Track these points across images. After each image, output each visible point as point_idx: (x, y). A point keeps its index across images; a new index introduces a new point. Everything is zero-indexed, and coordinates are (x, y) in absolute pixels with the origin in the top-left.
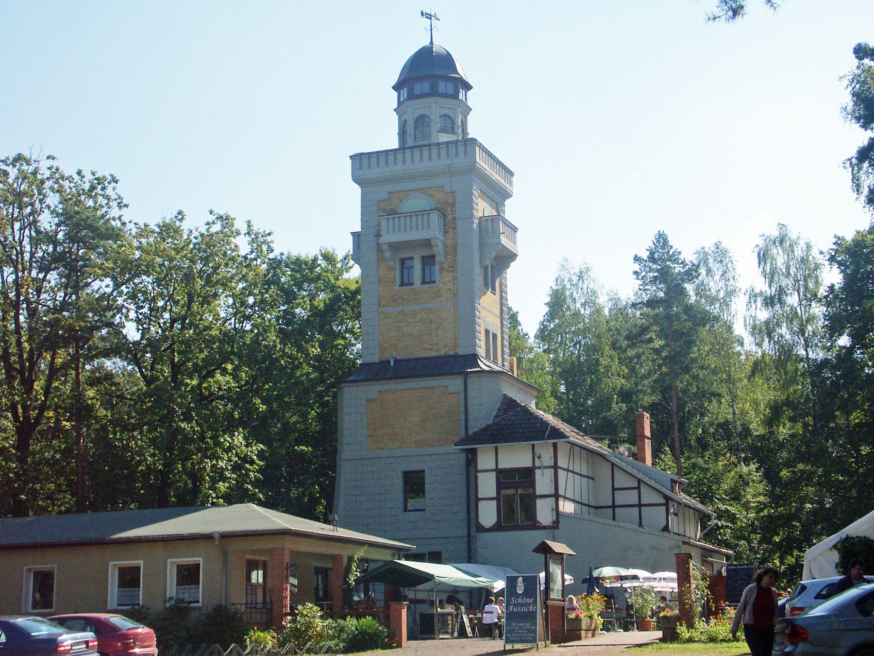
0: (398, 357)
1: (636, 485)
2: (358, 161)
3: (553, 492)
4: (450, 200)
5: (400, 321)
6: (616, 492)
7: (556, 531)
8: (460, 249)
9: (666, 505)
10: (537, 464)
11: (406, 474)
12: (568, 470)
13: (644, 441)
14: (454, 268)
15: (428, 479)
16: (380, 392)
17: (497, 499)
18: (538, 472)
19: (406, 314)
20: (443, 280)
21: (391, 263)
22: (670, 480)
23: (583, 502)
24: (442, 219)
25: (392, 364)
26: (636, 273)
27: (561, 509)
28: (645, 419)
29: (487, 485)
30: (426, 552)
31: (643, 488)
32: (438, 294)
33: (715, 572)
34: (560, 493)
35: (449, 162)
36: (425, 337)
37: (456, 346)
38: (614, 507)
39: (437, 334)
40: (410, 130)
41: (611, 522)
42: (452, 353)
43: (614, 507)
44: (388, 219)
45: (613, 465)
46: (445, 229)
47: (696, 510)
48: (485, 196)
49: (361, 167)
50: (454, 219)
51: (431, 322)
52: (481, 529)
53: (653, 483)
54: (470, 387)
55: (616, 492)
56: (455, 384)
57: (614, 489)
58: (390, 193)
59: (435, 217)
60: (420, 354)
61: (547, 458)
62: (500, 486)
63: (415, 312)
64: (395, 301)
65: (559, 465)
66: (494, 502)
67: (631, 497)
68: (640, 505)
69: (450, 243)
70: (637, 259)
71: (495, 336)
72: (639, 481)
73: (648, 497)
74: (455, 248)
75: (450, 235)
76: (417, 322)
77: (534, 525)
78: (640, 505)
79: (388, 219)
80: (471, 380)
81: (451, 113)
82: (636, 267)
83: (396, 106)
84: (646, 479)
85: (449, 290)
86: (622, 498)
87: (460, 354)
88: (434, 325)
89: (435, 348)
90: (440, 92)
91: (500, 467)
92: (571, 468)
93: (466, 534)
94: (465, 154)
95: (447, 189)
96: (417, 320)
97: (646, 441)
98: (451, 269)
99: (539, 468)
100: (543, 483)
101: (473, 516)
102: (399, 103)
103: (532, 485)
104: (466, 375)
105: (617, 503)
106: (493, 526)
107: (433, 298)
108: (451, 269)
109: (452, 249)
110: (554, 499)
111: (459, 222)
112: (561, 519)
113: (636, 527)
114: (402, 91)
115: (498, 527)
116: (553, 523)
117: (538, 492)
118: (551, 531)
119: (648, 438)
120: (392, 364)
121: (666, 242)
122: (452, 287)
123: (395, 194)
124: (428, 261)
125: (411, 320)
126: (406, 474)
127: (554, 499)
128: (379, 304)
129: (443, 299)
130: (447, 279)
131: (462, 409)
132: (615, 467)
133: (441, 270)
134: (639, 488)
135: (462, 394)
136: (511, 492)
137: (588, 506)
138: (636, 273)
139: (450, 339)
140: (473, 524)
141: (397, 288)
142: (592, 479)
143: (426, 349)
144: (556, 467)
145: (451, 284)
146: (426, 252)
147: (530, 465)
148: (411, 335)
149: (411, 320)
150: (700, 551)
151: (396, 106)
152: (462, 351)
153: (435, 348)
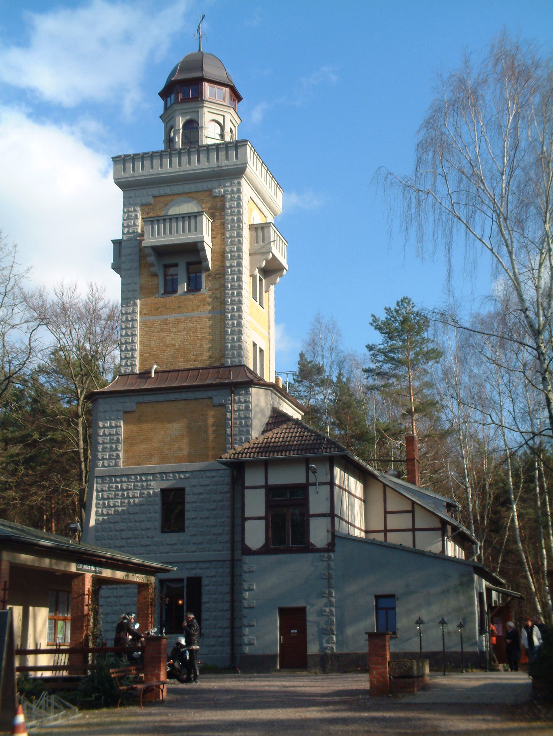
1: (410, 508)
3: (329, 512)
5: (162, 330)
6: (388, 515)
10: (312, 479)
11: (181, 529)
15: (188, 498)
18: (312, 489)
19: (169, 323)
27: (337, 528)
30: (185, 577)
31: (418, 512)
34: (336, 512)
37: (222, 357)
40: (211, 696)
44: (152, 221)
45: (385, 486)
49: (257, 242)
51: (196, 331)
52: (247, 551)
55: (388, 515)
57: (386, 513)
62: (269, 506)
63: (179, 322)
64: (158, 309)
68: (414, 530)
72: (413, 503)
76: (181, 331)
77: (309, 548)
82: (386, 311)
83: (163, 112)
90: (207, 141)
91: (270, 482)
93: (229, 557)
96: (180, 329)
98: (218, 276)
99: (314, 484)
101: (238, 538)
102: (166, 108)
103: (305, 503)
106: (260, 548)
107: (198, 306)
108: (218, 276)
110: (329, 518)
112: (337, 541)
114: (169, 99)
115: (265, 550)
116: (329, 544)
123: (160, 199)
126: (181, 529)
127: (329, 518)
132: (387, 488)
134: (412, 512)
140: (238, 546)
143: (189, 361)
147: (303, 480)
149: (174, 330)
151: (162, 111)
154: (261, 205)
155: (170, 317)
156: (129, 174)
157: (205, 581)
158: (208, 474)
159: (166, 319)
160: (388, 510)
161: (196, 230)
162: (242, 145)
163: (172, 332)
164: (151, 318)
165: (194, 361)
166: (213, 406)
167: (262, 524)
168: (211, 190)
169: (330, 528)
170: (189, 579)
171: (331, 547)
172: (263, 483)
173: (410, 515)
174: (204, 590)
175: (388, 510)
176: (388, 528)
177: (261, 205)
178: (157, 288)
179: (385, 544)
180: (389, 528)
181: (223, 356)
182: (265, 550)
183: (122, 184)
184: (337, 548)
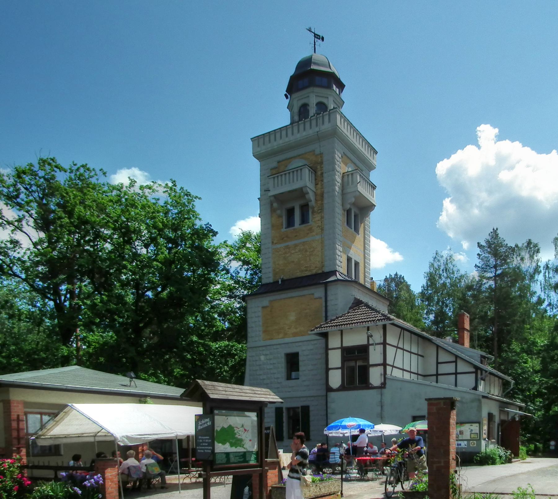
0: (285, 278)
1: (453, 359)
2: (256, 142)
4: (320, 160)
6: (439, 365)
7: (384, 390)
8: (326, 196)
9: (476, 373)
12: (397, 347)
13: (464, 332)
14: (321, 209)
16: (271, 302)
17: (342, 368)
18: (371, 348)
20: (314, 220)
21: (279, 212)
22: (480, 356)
23: (419, 373)
24: (313, 175)
25: (280, 283)
26: (478, 254)
28: (465, 317)
29: (335, 359)
31: (460, 363)
32: (311, 230)
33: (510, 418)
35: (317, 129)
36: (302, 262)
38: (437, 375)
39: (310, 260)
41: (434, 384)
42: (320, 272)
43: (437, 375)
44: (274, 178)
45: (438, 347)
46: (316, 182)
47: (499, 378)
48: (346, 158)
49: (258, 146)
50: (322, 174)
51: (306, 251)
53: (467, 358)
54: (329, 293)
55: (439, 365)
56: (319, 292)
57: (438, 363)
58: (279, 162)
59: (306, 172)
60: (299, 274)
61: (378, 337)
62: (344, 360)
63: (296, 246)
64: (283, 239)
65: (388, 341)
66: (340, 371)
67: (450, 368)
68: (456, 374)
69: (319, 192)
70: (480, 246)
71: (357, 264)
72: (457, 357)
73: (462, 367)
74: (322, 195)
75: (319, 186)
76: (296, 252)
78: (456, 374)
79: (274, 178)
80: (332, 290)
81: (324, 100)
84: (463, 356)
85: (318, 226)
86: (443, 369)
87: (325, 271)
88: (308, 253)
89: (308, 269)
91: (345, 345)
92: (400, 345)
94: (329, 121)
95: (317, 152)
97: (466, 332)
98: (320, 211)
99: (372, 344)
100: (375, 356)
103: (367, 358)
104: (326, 284)
105: (440, 372)
107: (308, 234)
108: (320, 211)
109: (320, 197)
111: (325, 175)
112: (387, 381)
113: (453, 387)
115: (342, 388)
116: (382, 384)
117: (371, 362)
118: (380, 390)
119: (467, 330)
120: (280, 283)
121: (497, 235)
122: (320, 224)
124: (305, 208)
125: (293, 252)
128: (273, 242)
129: (314, 233)
130: (317, 219)
131: (324, 309)
133: (313, 212)
134: (456, 362)
135: (324, 299)
136: (352, 364)
137: (418, 374)
138: (478, 254)
139: (319, 262)
141: (284, 230)
142: (422, 356)
144: (384, 344)
145: (320, 222)
146: (302, 202)
147: (365, 342)
148: (293, 262)
149: (293, 252)
150: (497, 403)
152: (326, 270)
153: (308, 269)
154: (352, 157)
155: (291, 243)
156: (263, 149)
157: (311, 409)
158: (312, 342)
159: (288, 245)
160: (439, 361)
161: (301, 179)
162: (333, 112)
163: (293, 253)
164: (279, 246)
165: (306, 271)
166: (315, 299)
167: (339, 372)
168: (314, 151)
169: (383, 373)
170: (302, 407)
171: (383, 386)
172: (340, 346)
173: (454, 364)
174: (311, 414)
175: (439, 361)
176: (454, 376)
177: (352, 157)
178: (282, 225)
179: (391, 378)
180: (454, 376)
181: (323, 266)
182: (342, 388)
183: (258, 156)
184: (387, 386)
